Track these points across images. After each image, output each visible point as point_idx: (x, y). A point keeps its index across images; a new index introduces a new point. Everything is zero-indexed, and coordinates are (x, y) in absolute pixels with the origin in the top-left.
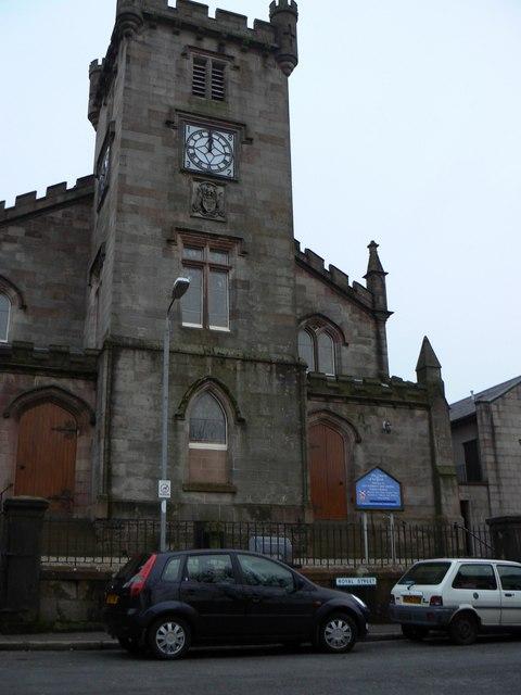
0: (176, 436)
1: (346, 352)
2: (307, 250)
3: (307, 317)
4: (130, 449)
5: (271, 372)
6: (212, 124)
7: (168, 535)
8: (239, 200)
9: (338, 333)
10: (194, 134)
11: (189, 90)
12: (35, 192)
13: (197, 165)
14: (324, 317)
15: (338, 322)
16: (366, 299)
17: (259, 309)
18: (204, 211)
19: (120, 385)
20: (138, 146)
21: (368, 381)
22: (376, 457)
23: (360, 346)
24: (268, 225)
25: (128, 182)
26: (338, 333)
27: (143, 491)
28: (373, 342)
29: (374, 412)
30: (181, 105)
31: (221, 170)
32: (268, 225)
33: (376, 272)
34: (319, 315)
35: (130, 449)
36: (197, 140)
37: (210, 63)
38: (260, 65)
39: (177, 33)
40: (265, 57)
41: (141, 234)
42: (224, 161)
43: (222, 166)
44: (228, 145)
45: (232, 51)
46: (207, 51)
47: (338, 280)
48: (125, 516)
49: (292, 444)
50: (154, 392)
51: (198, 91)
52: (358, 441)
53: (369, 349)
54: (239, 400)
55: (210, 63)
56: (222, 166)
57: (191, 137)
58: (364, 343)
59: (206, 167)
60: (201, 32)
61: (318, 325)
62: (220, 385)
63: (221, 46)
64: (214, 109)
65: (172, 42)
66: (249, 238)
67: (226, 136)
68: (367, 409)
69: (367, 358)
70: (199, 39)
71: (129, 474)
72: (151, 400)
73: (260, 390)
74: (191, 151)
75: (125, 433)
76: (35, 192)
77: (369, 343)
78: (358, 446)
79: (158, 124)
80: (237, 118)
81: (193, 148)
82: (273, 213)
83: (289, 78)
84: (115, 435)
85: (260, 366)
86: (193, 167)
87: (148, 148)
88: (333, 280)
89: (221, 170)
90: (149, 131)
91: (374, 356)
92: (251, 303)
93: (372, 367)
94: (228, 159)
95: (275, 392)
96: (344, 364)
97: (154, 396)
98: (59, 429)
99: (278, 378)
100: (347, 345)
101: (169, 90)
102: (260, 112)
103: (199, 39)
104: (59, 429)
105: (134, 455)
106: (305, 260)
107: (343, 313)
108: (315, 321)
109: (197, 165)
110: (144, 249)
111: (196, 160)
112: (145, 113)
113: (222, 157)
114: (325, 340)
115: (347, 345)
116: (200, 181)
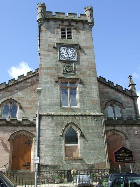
0: (60, 142)
1: (124, 111)
2: (108, 81)
3: (110, 101)
4: (46, 147)
5: (92, 118)
6: (68, 46)
7: (38, 179)
8: (78, 67)
9: (121, 105)
10: (62, 49)
11: (60, 37)
12: (23, 75)
13: (64, 58)
14: (116, 101)
15: (120, 102)
16: (129, 93)
17: (87, 99)
18: (67, 71)
19: (42, 128)
20: (45, 55)
21: (128, 118)
22: (133, 144)
23: (129, 108)
24: (88, 73)
25: (43, 66)
26: (121, 105)
27: (50, 161)
28: (133, 106)
29: (131, 129)
30: (58, 42)
31: (72, 59)
32: (88, 73)
33: (132, 85)
34: (114, 100)
35: (46, 147)
36: (63, 51)
37: (66, 29)
38: (82, 27)
39: (55, 22)
40: (84, 24)
41: (47, 81)
42: (73, 56)
43: (72, 57)
44: (74, 51)
45: (73, 24)
46: (65, 25)
47: (119, 89)
48: (44, 170)
49: (101, 142)
50: (53, 128)
51: (63, 37)
52: (127, 139)
53: (132, 109)
54: (81, 129)
55: (66, 29)
56: (72, 57)
57: (62, 50)
58: (130, 107)
59: (67, 58)
60: (63, 20)
61: (114, 103)
62: (74, 124)
63: (70, 23)
64: (69, 41)
65: (54, 24)
66: (82, 78)
67: (73, 48)
68: (129, 128)
69: (131, 112)
70: (63, 22)
71: (45, 156)
72: (52, 131)
73: (89, 125)
74: (62, 54)
75: (43, 143)
76: (23, 75)
77: (131, 107)
78: (127, 140)
79: (51, 48)
80: (76, 43)
81: (62, 53)
82: (89, 69)
83: (92, 29)
84: (40, 144)
85: (88, 117)
86: (63, 59)
87: (49, 55)
88: (118, 89)
89: (72, 59)
90: (48, 51)
91: (134, 111)
92: (84, 98)
93: (134, 115)
94: (74, 55)
95: (93, 125)
96: (124, 115)
97: (53, 130)
98: (26, 143)
99: (95, 121)
100: (124, 108)
101: (54, 38)
102: (83, 40)
103: (63, 22)
104: (26, 143)
105: (47, 149)
106: (108, 84)
107: (122, 98)
108: (113, 102)
109: (64, 58)
110: (48, 85)
111: (64, 57)
112: (47, 45)
113: (72, 55)
114: (117, 108)
115: (124, 108)
116: (65, 63)
